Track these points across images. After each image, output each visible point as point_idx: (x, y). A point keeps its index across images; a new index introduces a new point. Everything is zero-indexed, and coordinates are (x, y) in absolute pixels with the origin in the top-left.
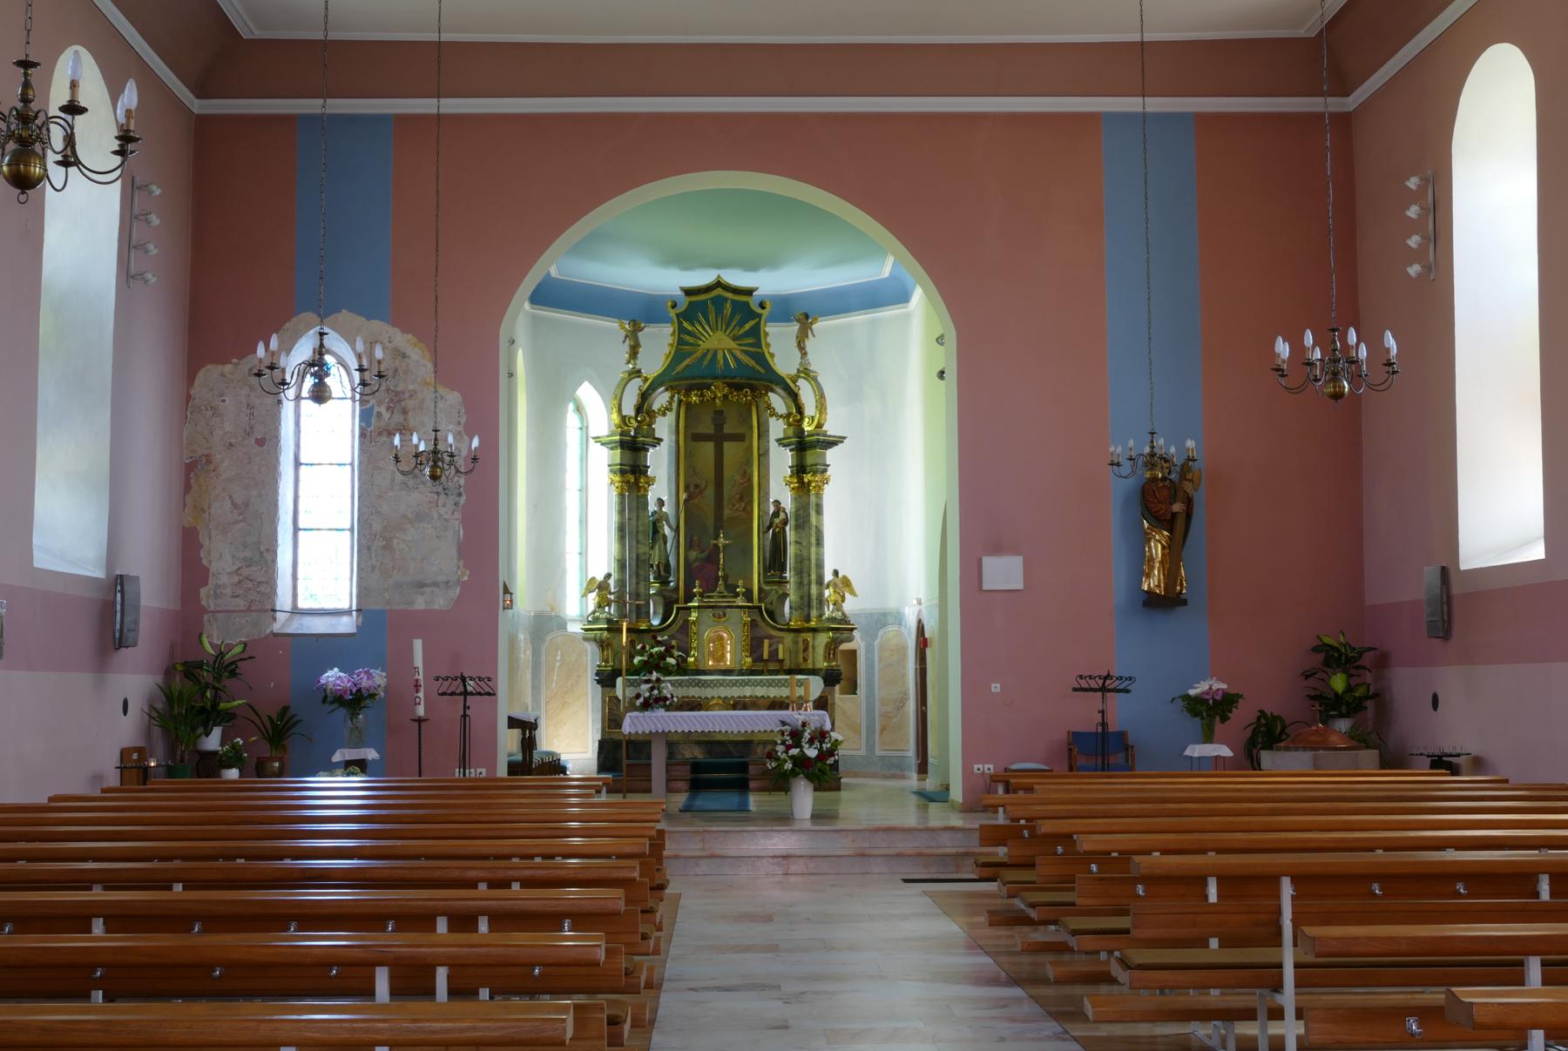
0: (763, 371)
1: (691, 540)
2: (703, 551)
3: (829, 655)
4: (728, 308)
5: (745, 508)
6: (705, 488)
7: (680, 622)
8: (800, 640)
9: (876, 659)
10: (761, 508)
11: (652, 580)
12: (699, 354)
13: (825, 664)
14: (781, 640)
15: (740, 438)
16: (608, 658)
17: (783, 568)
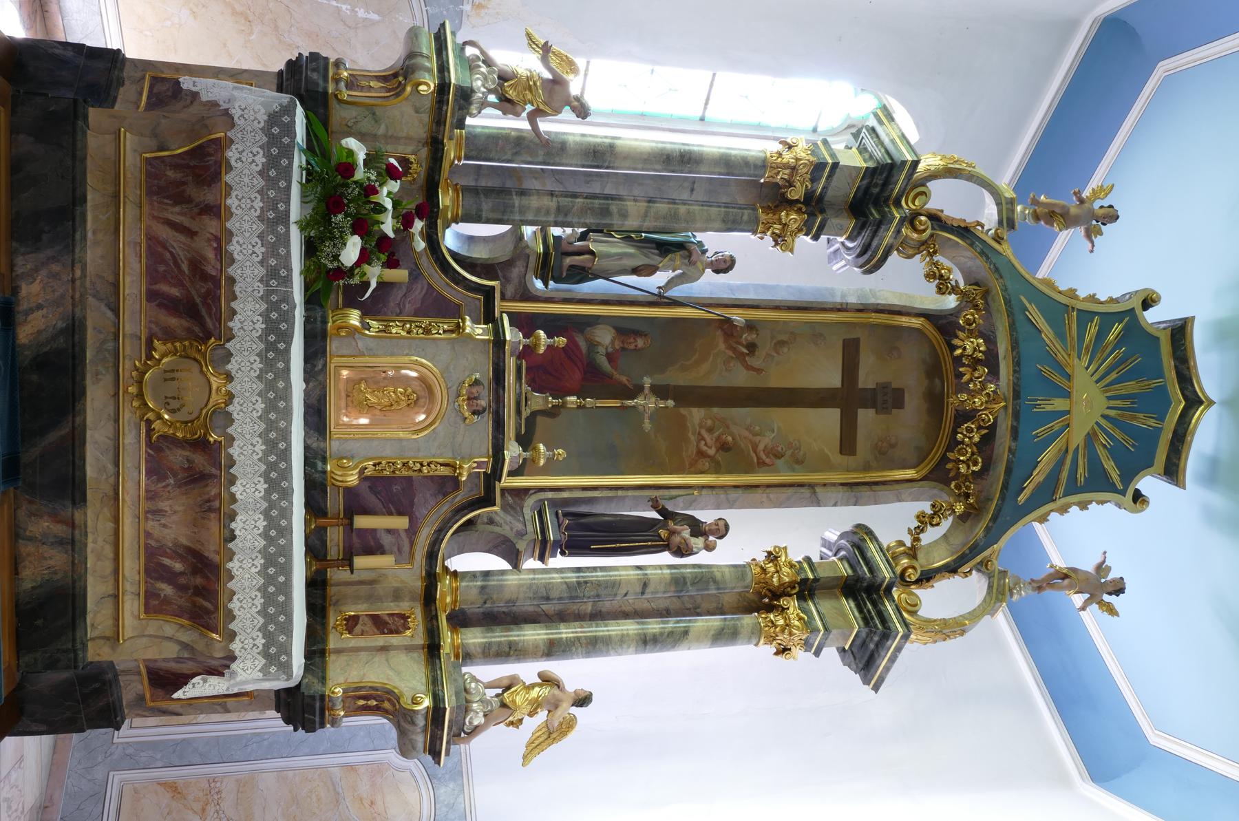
0: (1022, 498)
1: (637, 333)
2: (610, 357)
3: (365, 698)
4: (1144, 422)
5: (701, 454)
6: (749, 368)
7: (454, 294)
8: (403, 607)
9: (351, 758)
10: (704, 492)
11: (556, 231)
12: (1061, 356)
13: (339, 691)
14: (404, 555)
15: (847, 444)
16: (362, 89)
17: (574, 547)
